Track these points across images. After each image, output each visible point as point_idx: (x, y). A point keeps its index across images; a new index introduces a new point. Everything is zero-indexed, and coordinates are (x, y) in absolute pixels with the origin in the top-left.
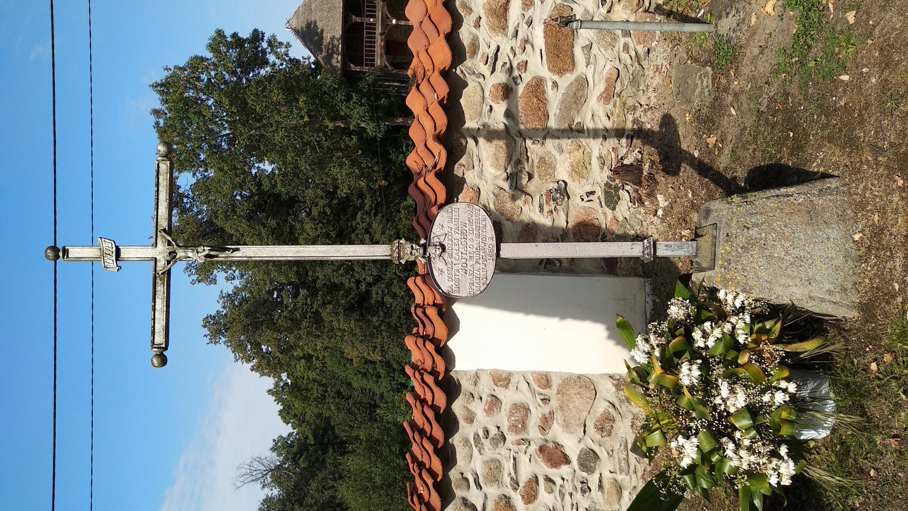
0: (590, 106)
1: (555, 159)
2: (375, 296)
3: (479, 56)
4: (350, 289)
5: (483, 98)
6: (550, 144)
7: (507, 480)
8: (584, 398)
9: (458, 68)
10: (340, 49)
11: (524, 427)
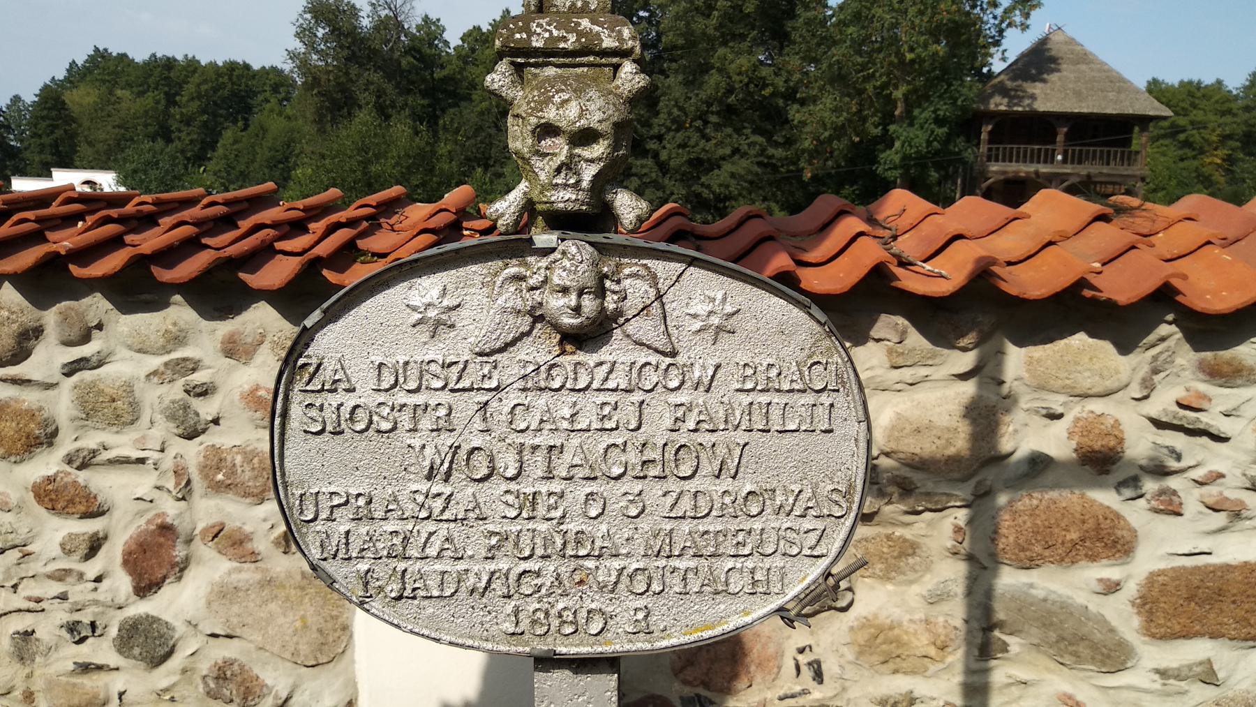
0: (1048, 676)
1: (911, 582)
2: (638, 163)
3: (1203, 387)
4: (650, 126)
5: (1085, 396)
6: (954, 573)
7: (91, 441)
8: (295, 639)
9: (1174, 328)
10: (1015, 109)
11: (218, 488)
